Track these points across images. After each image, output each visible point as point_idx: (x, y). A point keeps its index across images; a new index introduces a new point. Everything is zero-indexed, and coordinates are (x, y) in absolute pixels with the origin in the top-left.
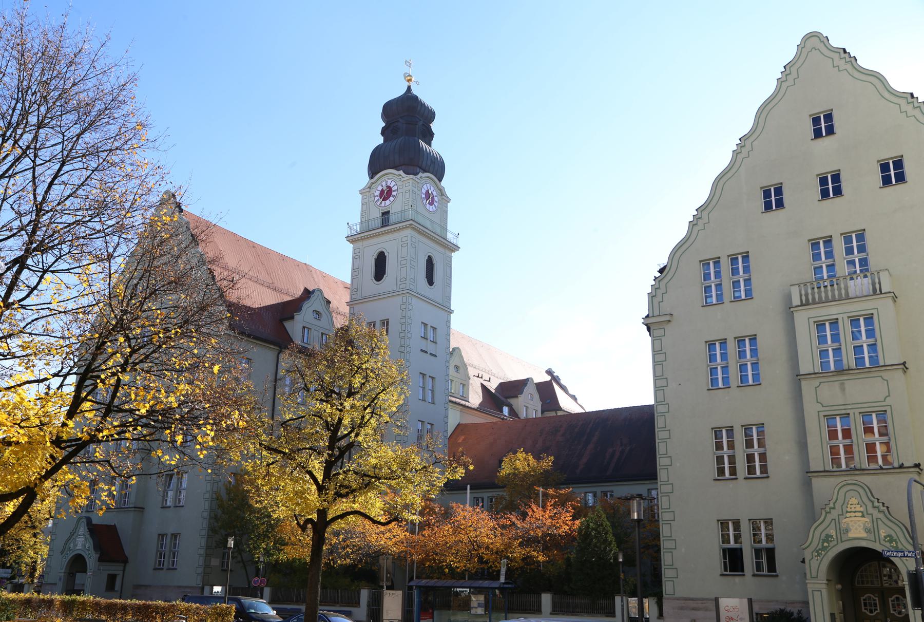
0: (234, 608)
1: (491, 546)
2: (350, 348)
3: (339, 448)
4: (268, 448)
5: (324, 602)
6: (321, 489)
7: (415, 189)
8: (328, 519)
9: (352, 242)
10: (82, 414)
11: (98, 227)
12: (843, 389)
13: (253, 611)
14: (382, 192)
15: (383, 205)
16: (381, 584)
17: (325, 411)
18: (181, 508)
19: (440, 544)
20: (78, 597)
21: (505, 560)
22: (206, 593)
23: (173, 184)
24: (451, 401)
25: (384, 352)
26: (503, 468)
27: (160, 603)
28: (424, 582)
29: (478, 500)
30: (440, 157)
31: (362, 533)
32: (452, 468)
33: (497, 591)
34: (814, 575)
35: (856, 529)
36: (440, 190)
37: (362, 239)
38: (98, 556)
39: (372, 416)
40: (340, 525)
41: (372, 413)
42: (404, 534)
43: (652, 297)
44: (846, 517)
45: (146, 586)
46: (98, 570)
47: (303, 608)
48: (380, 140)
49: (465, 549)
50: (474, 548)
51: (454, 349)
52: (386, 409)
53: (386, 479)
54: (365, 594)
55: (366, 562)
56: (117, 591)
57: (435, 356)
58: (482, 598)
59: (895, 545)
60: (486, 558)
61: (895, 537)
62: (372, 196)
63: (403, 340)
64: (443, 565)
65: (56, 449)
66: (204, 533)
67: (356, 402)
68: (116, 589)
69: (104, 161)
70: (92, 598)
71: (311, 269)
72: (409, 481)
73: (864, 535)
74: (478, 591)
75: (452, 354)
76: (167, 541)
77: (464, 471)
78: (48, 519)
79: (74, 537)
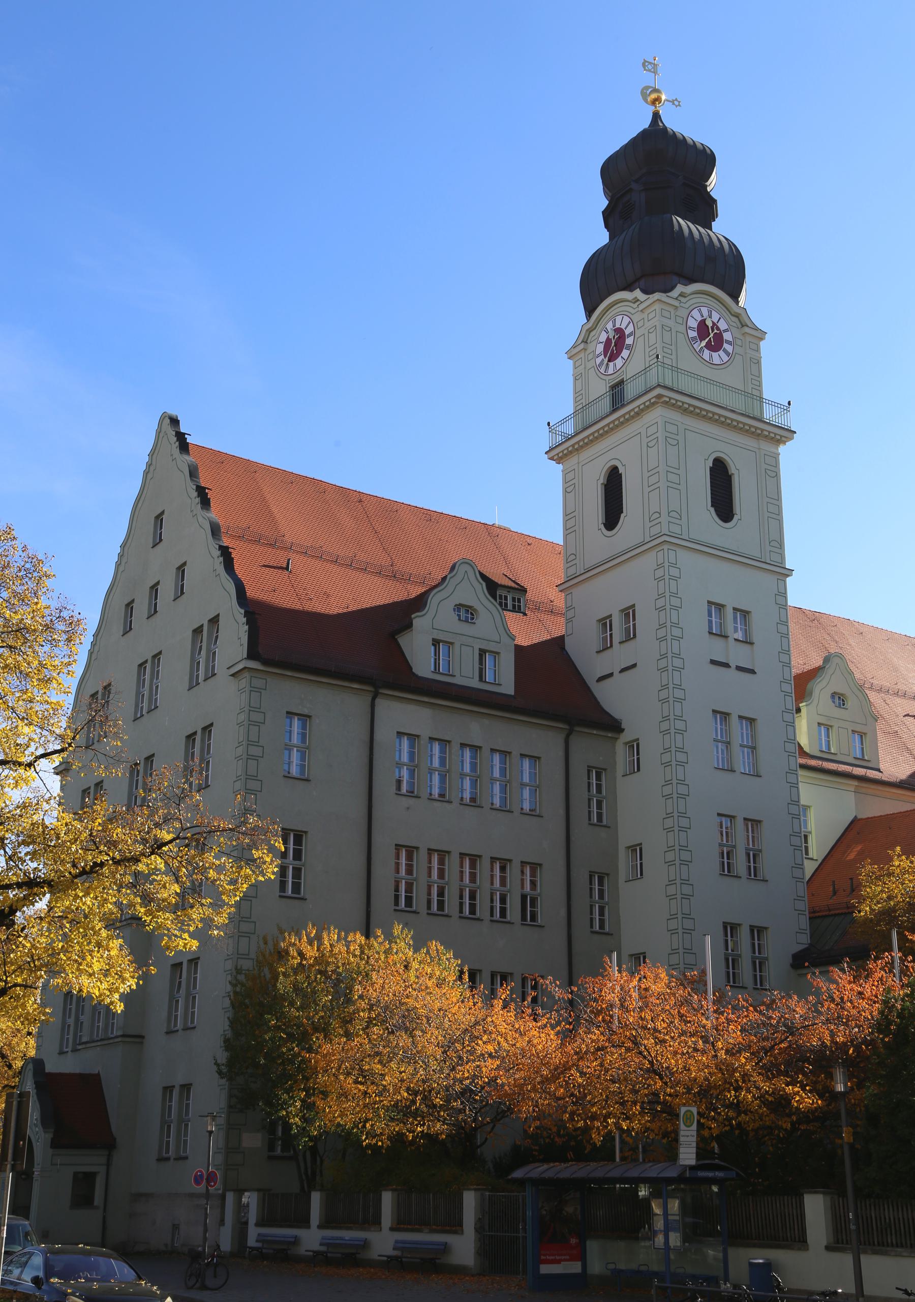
7: (671, 323)
9: (559, 460)
15: (611, 371)
36: (737, 316)
38: (50, 1136)
48: (602, 237)
57: (752, 672)
62: (591, 356)
68: (96, 1203)
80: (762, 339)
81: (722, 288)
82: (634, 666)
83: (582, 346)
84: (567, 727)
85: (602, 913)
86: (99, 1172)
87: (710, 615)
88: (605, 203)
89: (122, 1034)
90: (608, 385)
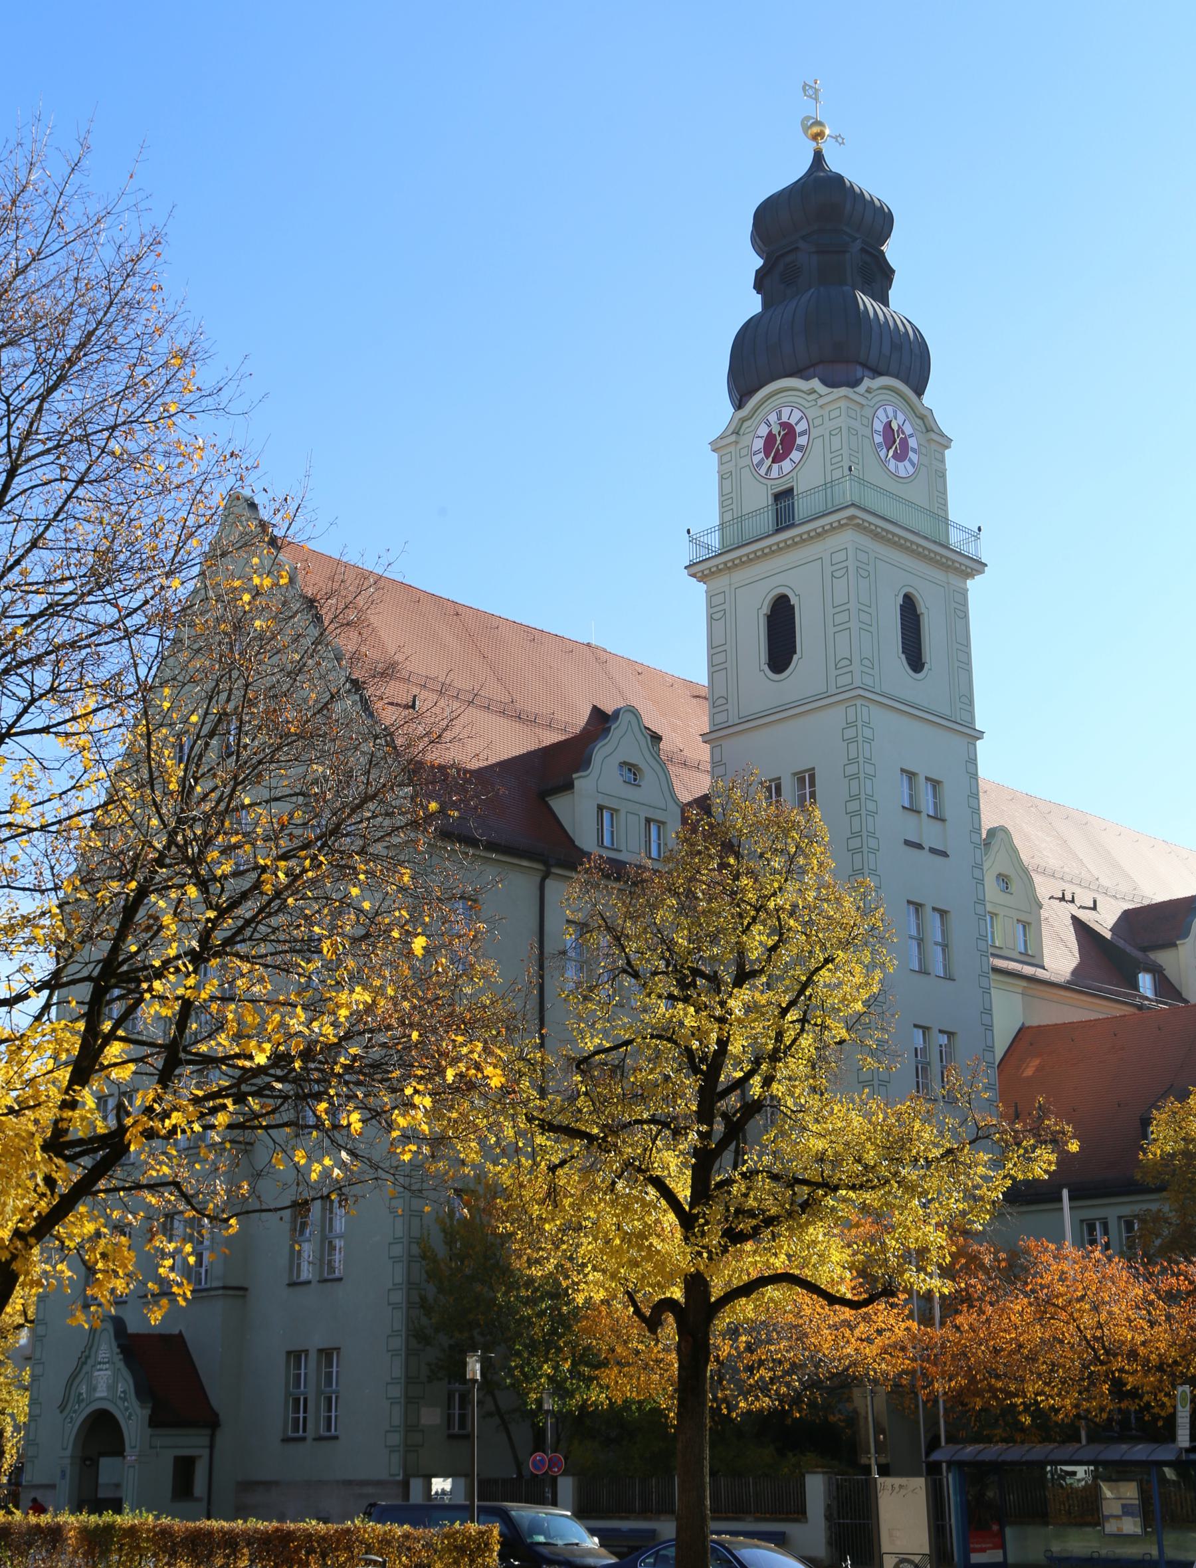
0: (496, 1532)
1: (1142, 1351)
2: (732, 861)
3: (725, 1115)
4: (548, 1127)
5: (719, 1513)
6: (687, 1221)
7: (856, 424)
8: (713, 1299)
9: (702, 577)
10: (103, 1074)
11: (108, 614)
13: (541, 1539)
14: (770, 439)
15: (774, 473)
16: (864, 1461)
17: (681, 1024)
18: (336, 1284)
19: (1003, 1349)
20: (118, 1519)
21: (1187, 1388)
22: (416, 1497)
23: (271, 495)
24: (996, 970)
25: (821, 864)
26: (1155, 1140)
27: (312, 1525)
28: (969, 1451)
29: (1091, 1229)
30: (915, 329)
31: (796, 1327)
32: (1021, 1151)
33: (1169, 1473)
36: (922, 418)
37: (729, 568)
38: (147, 1412)
39: (802, 1030)
40: (745, 1309)
41: (803, 1021)
42: (903, 1326)
45: (268, 1485)
46: (151, 1447)
47: (667, 1529)
48: (753, 305)
49: (1073, 1361)
50: (1097, 1357)
51: (992, 832)
52: (839, 1010)
53: (853, 1188)
54: (816, 1487)
55: (812, 1404)
56: (198, 1500)
57: (944, 854)
58: (1130, 1491)
60: (1131, 1382)
62: (744, 452)
63: (856, 820)
64: (1014, 1405)
65: (55, 1159)
66: (398, 1343)
67: (757, 995)
69: (103, 452)
70: (151, 1518)
71: (604, 657)
72: (910, 1188)
73: (104, 1394)
74: (1118, 1471)
75: (987, 844)
76: (310, 1367)
77: (1053, 1157)
78: (20, 1326)
79: (86, 1368)
80: (947, 447)
81: (906, 382)
83: (733, 438)
84: (540, 867)
86: (200, 1457)
89: (221, 1285)
90: (770, 492)
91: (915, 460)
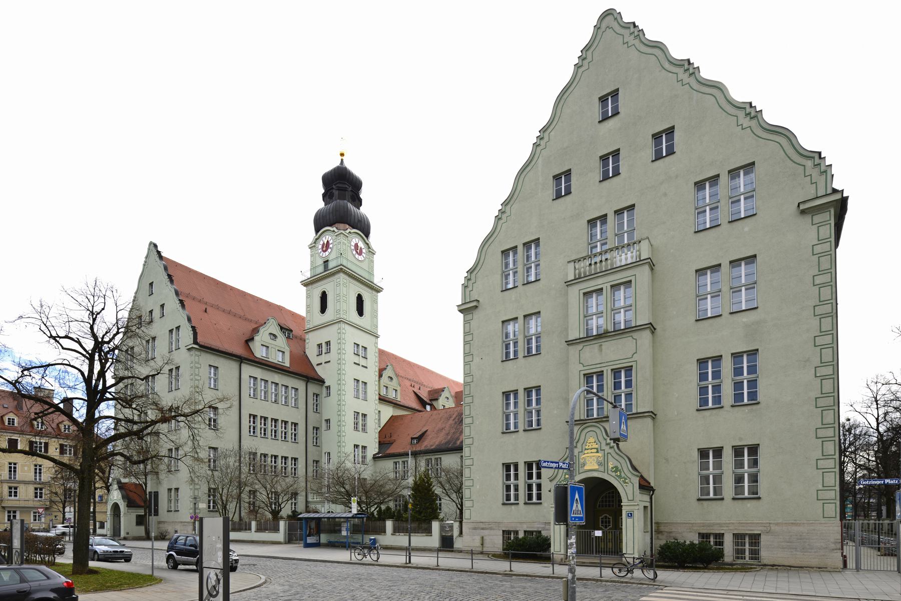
12: (601, 350)
30: (366, 216)
34: (630, 498)
35: (591, 463)
36: (367, 244)
43: (465, 287)
44: (585, 454)
57: (366, 367)
59: (619, 474)
61: (620, 468)
73: (596, 467)
82: (329, 362)
85: (316, 439)
87: (354, 347)
88: (323, 191)
91: (365, 256)
